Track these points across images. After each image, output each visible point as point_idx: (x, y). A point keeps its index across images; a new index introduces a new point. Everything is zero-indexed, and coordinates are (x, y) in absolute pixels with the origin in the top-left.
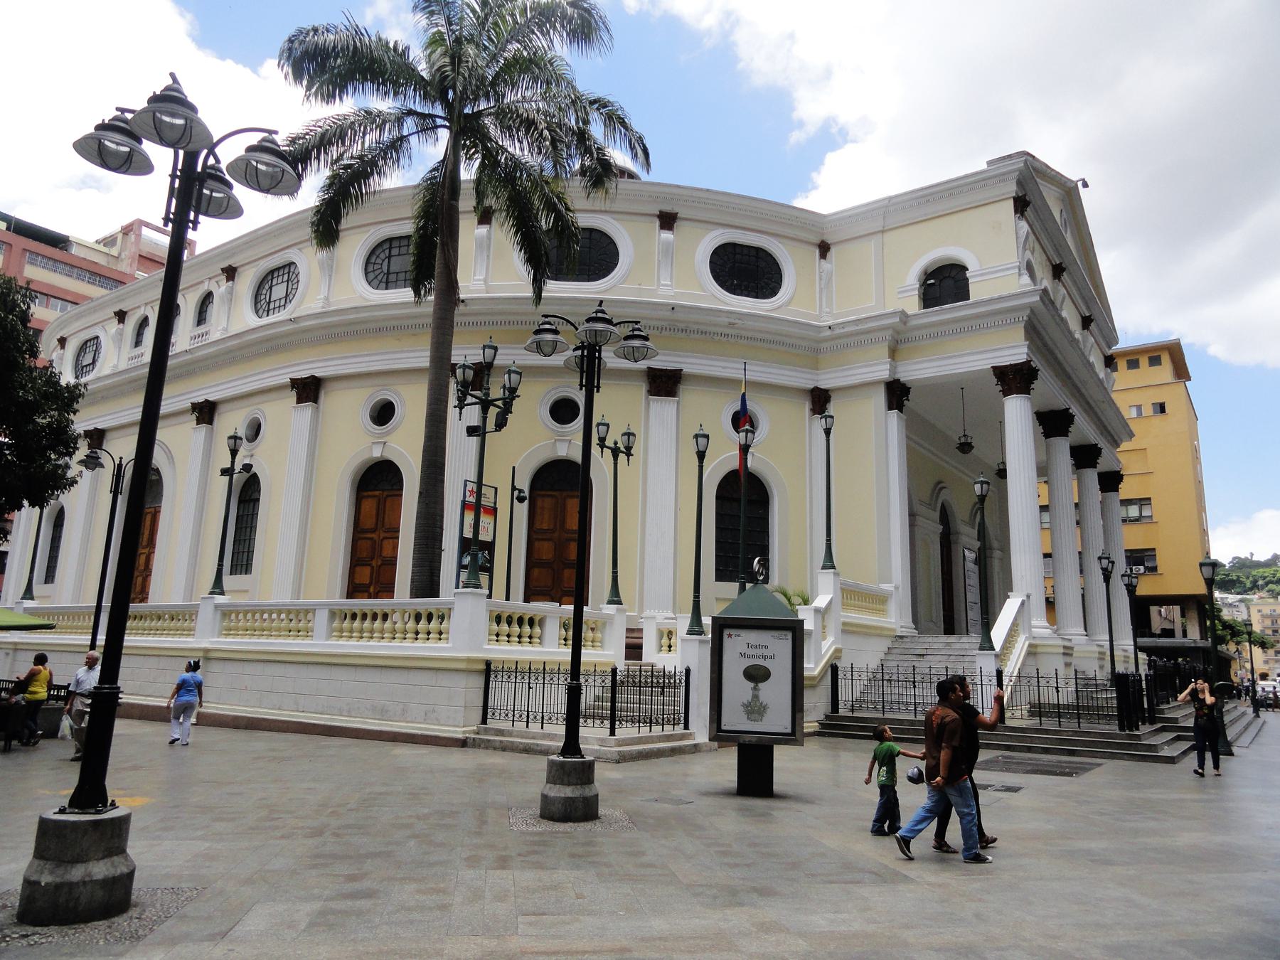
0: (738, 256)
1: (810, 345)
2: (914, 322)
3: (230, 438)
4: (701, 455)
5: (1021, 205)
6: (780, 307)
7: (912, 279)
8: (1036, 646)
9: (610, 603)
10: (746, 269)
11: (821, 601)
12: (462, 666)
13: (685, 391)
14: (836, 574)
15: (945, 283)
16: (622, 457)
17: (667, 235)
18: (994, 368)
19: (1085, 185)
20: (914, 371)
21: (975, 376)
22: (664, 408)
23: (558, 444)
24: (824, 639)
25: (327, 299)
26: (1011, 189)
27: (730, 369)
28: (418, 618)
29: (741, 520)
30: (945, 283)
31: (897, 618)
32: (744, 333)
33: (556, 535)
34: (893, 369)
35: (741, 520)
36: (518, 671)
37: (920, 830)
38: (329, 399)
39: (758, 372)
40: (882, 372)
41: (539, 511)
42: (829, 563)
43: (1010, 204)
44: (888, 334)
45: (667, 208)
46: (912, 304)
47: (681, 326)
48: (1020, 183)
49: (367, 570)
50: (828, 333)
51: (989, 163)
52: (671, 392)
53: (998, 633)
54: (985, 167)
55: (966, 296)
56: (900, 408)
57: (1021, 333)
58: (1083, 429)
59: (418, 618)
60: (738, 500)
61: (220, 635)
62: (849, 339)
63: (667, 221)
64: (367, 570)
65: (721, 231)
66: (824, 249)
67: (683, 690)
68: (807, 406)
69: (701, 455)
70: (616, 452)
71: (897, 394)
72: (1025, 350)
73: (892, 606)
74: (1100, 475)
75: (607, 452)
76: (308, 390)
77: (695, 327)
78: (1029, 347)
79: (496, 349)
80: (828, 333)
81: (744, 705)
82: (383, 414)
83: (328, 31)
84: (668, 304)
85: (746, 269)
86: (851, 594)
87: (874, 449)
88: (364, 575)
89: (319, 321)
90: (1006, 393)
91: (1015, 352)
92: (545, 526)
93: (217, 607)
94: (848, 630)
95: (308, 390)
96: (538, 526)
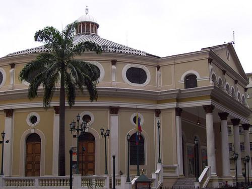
1: (157, 98)
5: (210, 61)
9: (105, 174)
10: (136, 75)
11: (157, 171)
15: (191, 80)
17: (114, 67)
19: (234, 43)
20: (184, 105)
26: (207, 56)
28: (61, 181)
30: (191, 80)
49: (31, 165)
50: (159, 94)
52: (116, 113)
53: (200, 179)
56: (180, 115)
59: (61, 181)
64: (31, 165)
66: (159, 68)
70: (105, 136)
71: (179, 111)
73: (177, 170)
80: (159, 94)
81: (230, 47)
82: (34, 119)
87: (174, 124)
88: (30, 167)
90: (207, 112)
94: (164, 178)
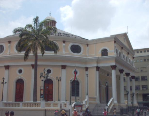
1: (85, 61)
3: (3, 79)
5: (115, 42)
7: (100, 52)
8: (115, 105)
10: (76, 49)
11: (86, 100)
12: (43, 110)
13: (67, 68)
14: (88, 96)
15: (104, 52)
16: (60, 81)
17: (64, 44)
19: (127, 33)
20: (100, 65)
21: (108, 67)
22: (64, 71)
24: (86, 105)
25: (9, 52)
26: (114, 40)
27: (74, 65)
29: (75, 88)
30: (104, 52)
31: (98, 101)
34: (97, 65)
35: (75, 88)
36: (49, 110)
38: (11, 69)
39: (78, 65)
40: (96, 65)
42: (87, 95)
43: (113, 42)
46: (100, 56)
53: (109, 104)
55: (107, 55)
57: (114, 61)
58: (126, 71)
60: (75, 84)
61: (4, 107)
62: (91, 61)
63: (64, 42)
66: (88, 45)
67: (69, 112)
68: (85, 70)
70: (59, 81)
71: (98, 68)
72: (115, 63)
75: (58, 81)
76: (7, 67)
78: (115, 63)
86: (90, 98)
90: (113, 69)
91: (113, 64)
93: (3, 103)
95: (7, 67)
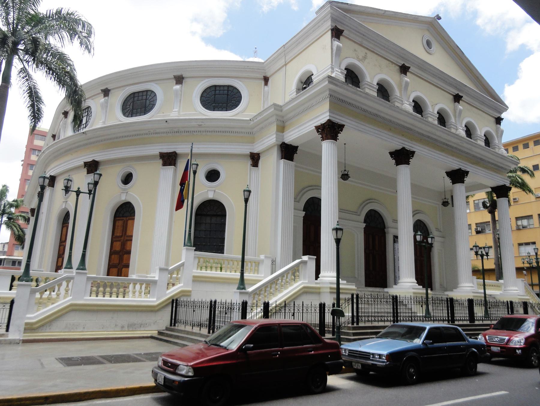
0: (217, 92)
1: (249, 131)
2: (285, 109)
4: (246, 200)
6: (238, 113)
18: (317, 128)
19: (439, 18)
23: (122, 195)
26: (328, 25)
32: (208, 129)
33: (122, 238)
37: (101, 357)
41: (116, 227)
44: (274, 118)
45: (178, 73)
47: (176, 130)
48: (333, 20)
51: (317, 13)
54: (315, 16)
63: (179, 80)
65: (207, 80)
66: (266, 80)
69: (246, 200)
74: (466, 187)
77: (183, 130)
79: (197, 165)
83: (84, 26)
84: (164, 120)
85: (221, 97)
89: (360, 185)
92: (118, 235)
96: (115, 235)
